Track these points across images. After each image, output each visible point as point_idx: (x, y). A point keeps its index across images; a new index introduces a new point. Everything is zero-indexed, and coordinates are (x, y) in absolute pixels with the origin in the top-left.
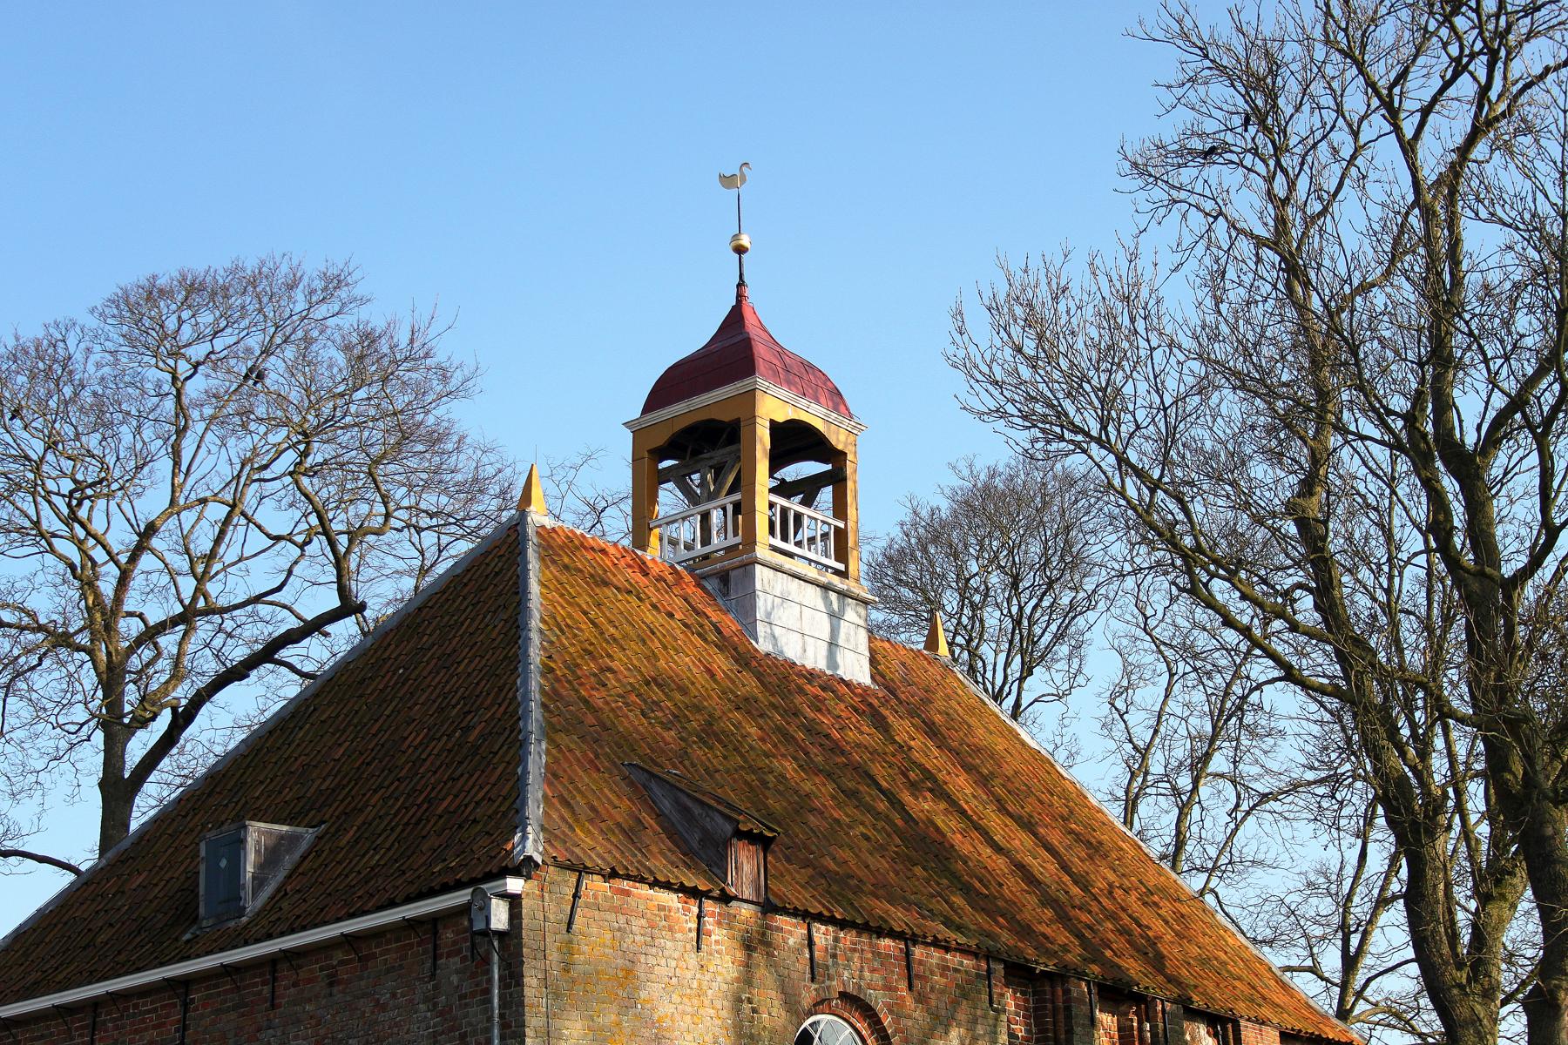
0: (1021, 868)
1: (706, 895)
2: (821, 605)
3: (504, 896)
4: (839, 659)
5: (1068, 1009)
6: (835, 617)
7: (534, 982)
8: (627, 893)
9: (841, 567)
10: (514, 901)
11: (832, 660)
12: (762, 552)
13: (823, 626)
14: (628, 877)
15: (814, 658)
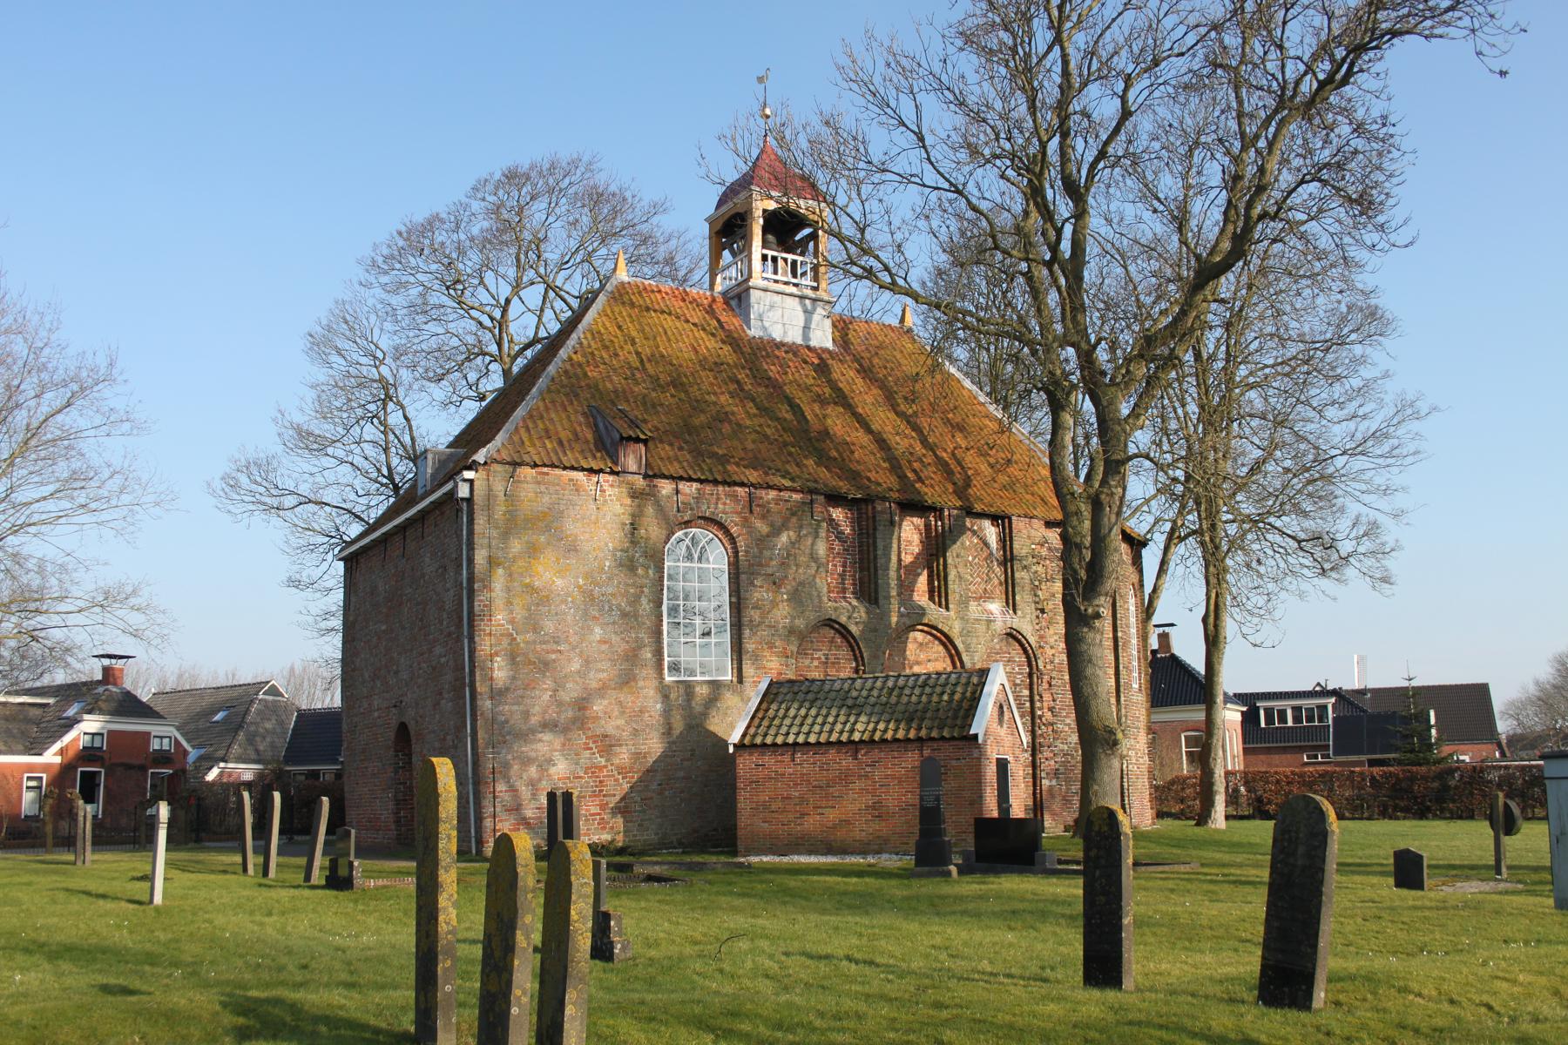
0: (881, 442)
1: (601, 471)
2: (799, 308)
3: (465, 480)
4: (811, 335)
5: (874, 517)
6: (808, 313)
7: (481, 522)
8: (547, 474)
9: (815, 284)
10: (471, 482)
11: (806, 336)
12: (756, 281)
13: (800, 318)
14: (545, 465)
15: (794, 336)
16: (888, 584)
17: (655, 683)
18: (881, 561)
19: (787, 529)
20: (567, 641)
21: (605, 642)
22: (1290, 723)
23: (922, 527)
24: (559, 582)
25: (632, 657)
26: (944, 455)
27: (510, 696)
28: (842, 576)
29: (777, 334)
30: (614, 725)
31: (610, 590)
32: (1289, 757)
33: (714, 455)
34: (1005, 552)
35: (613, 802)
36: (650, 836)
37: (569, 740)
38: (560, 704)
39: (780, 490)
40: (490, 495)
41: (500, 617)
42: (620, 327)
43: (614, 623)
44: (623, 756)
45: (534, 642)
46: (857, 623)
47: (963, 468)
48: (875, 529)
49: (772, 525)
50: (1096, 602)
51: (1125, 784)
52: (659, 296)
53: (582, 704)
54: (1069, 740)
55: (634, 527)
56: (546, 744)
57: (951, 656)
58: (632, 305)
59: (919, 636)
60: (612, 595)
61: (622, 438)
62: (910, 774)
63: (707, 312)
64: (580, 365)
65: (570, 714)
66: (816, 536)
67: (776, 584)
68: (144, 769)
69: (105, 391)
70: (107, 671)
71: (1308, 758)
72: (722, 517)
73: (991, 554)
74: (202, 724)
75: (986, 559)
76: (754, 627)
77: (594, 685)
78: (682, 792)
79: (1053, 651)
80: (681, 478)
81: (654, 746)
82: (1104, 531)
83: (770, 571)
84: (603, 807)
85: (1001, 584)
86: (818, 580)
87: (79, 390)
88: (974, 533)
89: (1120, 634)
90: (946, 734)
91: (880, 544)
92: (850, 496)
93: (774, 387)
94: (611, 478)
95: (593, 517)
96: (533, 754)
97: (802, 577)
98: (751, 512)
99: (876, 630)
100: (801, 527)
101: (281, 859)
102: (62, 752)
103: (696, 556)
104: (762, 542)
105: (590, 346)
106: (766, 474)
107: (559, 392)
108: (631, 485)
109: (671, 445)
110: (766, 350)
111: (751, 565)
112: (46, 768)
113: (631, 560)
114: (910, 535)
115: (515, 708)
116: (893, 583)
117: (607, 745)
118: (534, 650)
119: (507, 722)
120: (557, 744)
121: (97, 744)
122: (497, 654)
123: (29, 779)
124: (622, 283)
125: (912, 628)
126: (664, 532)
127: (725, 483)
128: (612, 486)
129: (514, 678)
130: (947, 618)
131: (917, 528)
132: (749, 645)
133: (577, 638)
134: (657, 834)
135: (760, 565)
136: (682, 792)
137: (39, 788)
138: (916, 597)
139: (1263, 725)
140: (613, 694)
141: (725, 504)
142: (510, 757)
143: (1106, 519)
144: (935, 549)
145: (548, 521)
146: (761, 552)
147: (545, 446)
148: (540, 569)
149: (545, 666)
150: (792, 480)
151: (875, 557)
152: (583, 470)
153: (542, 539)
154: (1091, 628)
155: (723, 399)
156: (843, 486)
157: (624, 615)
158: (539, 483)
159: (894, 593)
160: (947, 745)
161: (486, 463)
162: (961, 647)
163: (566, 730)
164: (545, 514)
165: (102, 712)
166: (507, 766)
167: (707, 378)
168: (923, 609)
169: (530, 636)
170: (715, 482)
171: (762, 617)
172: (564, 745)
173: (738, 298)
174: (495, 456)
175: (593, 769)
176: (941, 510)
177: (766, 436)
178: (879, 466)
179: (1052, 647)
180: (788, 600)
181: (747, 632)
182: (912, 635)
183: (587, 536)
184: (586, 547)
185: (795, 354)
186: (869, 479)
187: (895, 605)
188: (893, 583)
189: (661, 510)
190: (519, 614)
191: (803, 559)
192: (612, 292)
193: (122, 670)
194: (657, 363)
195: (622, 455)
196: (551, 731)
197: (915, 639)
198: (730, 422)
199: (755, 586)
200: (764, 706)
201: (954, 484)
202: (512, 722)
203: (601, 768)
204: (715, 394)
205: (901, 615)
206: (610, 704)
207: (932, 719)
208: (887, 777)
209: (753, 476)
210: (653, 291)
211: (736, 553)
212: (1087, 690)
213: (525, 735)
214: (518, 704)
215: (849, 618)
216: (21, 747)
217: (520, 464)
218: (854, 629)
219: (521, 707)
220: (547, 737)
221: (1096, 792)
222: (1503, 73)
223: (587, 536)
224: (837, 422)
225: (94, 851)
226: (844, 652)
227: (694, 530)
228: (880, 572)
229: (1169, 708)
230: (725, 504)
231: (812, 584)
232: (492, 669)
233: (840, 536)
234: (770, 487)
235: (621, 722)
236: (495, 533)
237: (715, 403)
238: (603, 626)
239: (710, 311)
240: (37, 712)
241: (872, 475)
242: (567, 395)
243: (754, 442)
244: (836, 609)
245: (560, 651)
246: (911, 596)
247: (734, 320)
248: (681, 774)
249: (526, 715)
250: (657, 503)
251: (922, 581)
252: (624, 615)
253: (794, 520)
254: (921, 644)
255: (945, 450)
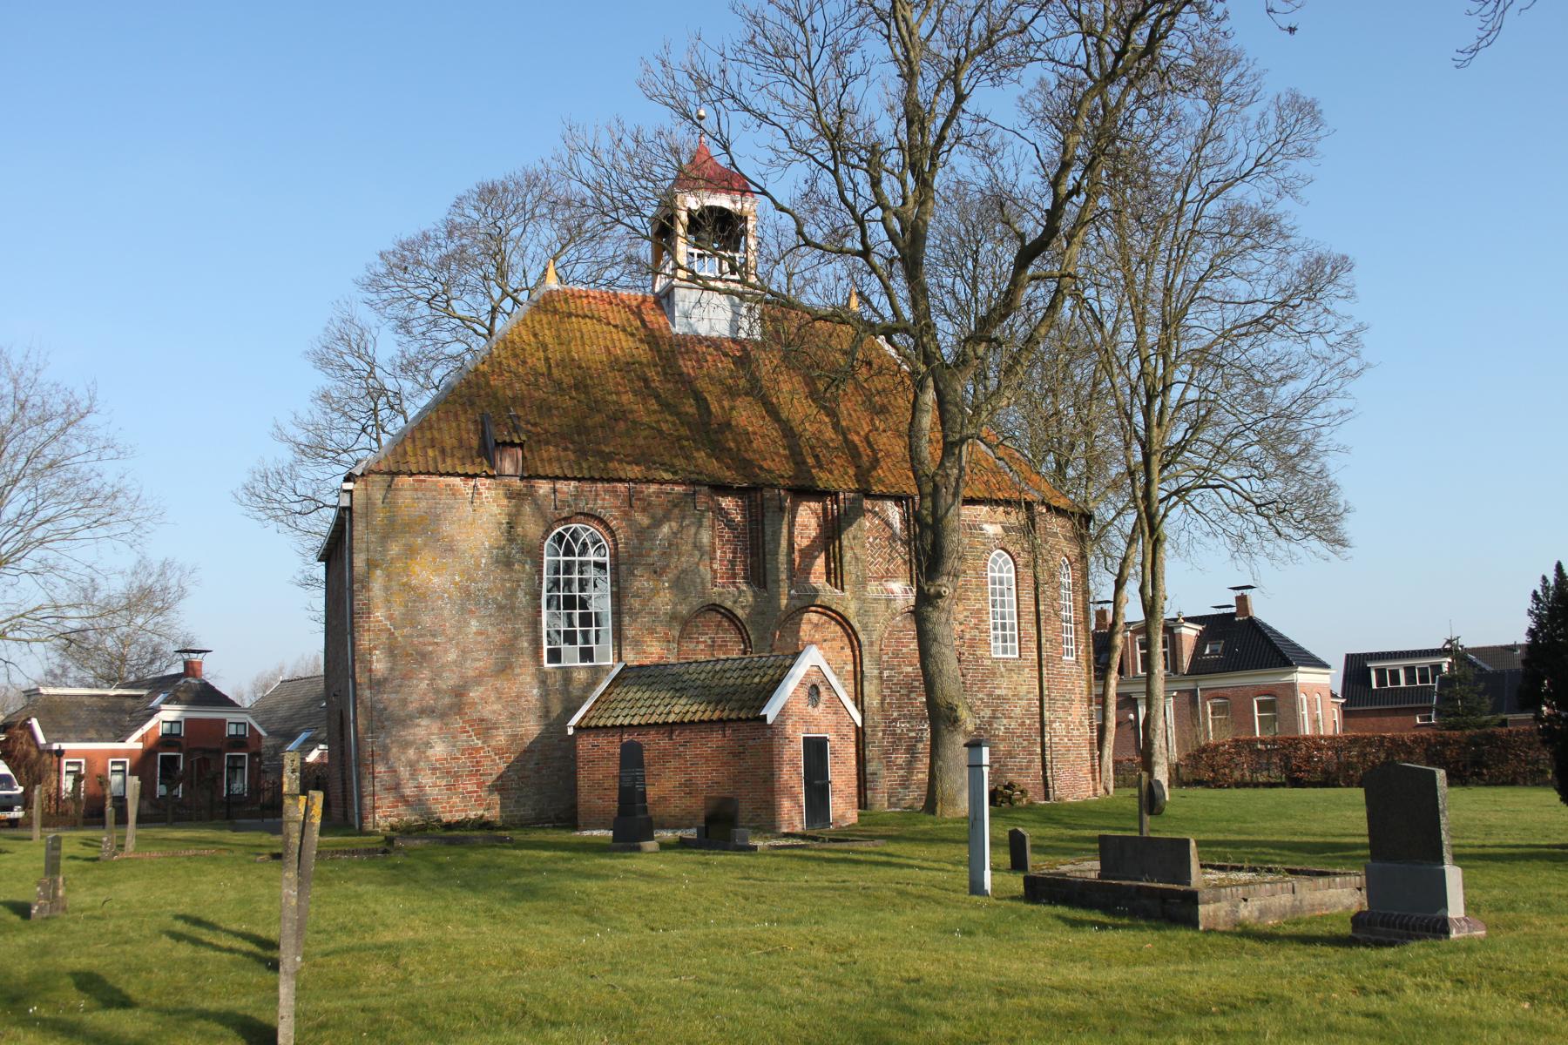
1: (475, 476)
8: (424, 481)
14: (420, 473)
16: (778, 568)
17: (531, 669)
18: (769, 547)
19: (669, 520)
20: (443, 633)
21: (481, 634)
22: (1403, 684)
23: (820, 511)
24: (435, 580)
25: (509, 647)
26: (856, 438)
27: (388, 687)
28: (732, 562)
29: (703, 329)
30: (491, 709)
31: (486, 585)
32: (1399, 720)
33: (600, 453)
34: (909, 531)
35: (490, 780)
36: (527, 811)
37: (446, 724)
38: (437, 691)
39: (662, 484)
40: (369, 504)
41: (379, 614)
42: (535, 335)
43: (490, 616)
44: (501, 738)
45: (411, 636)
46: (743, 607)
47: (873, 450)
48: (763, 516)
49: (653, 517)
50: (939, 582)
51: (1048, 758)
52: (585, 301)
53: (459, 692)
54: (982, 714)
55: (511, 526)
56: (424, 728)
57: (849, 636)
58: (555, 312)
59: (814, 617)
60: (488, 589)
61: (497, 444)
62: (716, 754)
63: (633, 313)
64: (484, 374)
65: (447, 700)
66: (700, 526)
67: (657, 573)
68: (220, 753)
69: (90, 420)
70: (187, 664)
71: (1422, 719)
72: (600, 512)
73: (894, 534)
74: (313, 710)
75: (888, 539)
76: (634, 615)
77: (471, 673)
78: (560, 770)
79: (962, 627)
80: (557, 478)
81: (532, 728)
82: (941, 512)
83: (650, 560)
84: (480, 785)
85: (905, 563)
86: (701, 567)
87: (73, 417)
88: (876, 514)
89: (1042, 608)
90: (743, 715)
91: (769, 531)
92: (735, 486)
93: (683, 383)
94: (488, 481)
95: (470, 519)
96: (411, 738)
97: (685, 565)
98: (631, 506)
99: (763, 613)
100: (684, 518)
101: (140, 832)
102: (143, 739)
103: (577, 551)
104: (643, 534)
105: (499, 356)
106: (649, 469)
107: (455, 402)
108: (507, 487)
109: (556, 446)
110: (686, 346)
111: (630, 556)
112: (129, 753)
113: (508, 556)
114: (807, 518)
115: (393, 696)
116: (783, 567)
117: (485, 728)
118: (412, 644)
119: (385, 709)
120: (435, 727)
121: (176, 731)
122: (375, 648)
123: (113, 763)
124: (551, 292)
125: (805, 609)
126: (542, 529)
127: (602, 480)
128: (488, 489)
129: (392, 669)
130: (843, 599)
131: (814, 512)
132: (630, 632)
133: (454, 631)
134: (534, 810)
135: (641, 555)
136: (560, 770)
137: (124, 771)
138: (812, 579)
139: (1374, 686)
140: (490, 682)
141: (605, 500)
142: (388, 741)
143: (942, 501)
144: (832, 532)
145: (427, 526)
146: (641, 544)
147: (426, 455)
148: (417, 569)
149: (423, 657)
150: (675, 473)
151: (764, 544)
152: (459, 475)
153: (419, 541)
154: (936, 607)
155: (624, 398)
156: (728, 475)
157: (500, 608)
158: (416, 490)
159: (783, 576)
160: (744, 726)
161: (363, 475)
162: (857, 626)
163: (443, 716)
164: (422, 518)
165: (179, 702)
166: (386, 749)
167: (613, 377)
168: (816, 590)
169: (407, 631)
170: (593, 480)
171: (644, 605)
172: (441, 729)
173: (665, 300)
174: (373, 467)
175: (472, 751)
176: (836, 494)
177: (660, 432)
178: (778, 454)
179: (961, 624)
180: (669, 588)
181: (626, 620)
182: (806, 616)
183: (464, 536)
184: (462, 546)
185: (717, 348)
186: (761, 468)
187: (784, 588)
188: (783, 567)
189: (538, 508)
190: (398, 611)
191: (686, 548)
192: (538, 301)
193: (200, 663)
194: (564, 367)
195: (498, 458)
196: (428, 716)
197: (810, 621)
198: (626, 420)
199: (634, 575)
200: (610, 690)
201: (858, 467)
202: (390, 709)
203: (478, 750)
204: (618, 393)
205: (791, 598)
206: (487, 690)
207: (737, 701)
208: (696, 756)
209: (635, 471)
210: (581, 297)
211: (616, 545)
212: (932, 668)
213: (404, 722)
214: (397, 692)
215: (735, 602)
216: (111, 735)
217: (399, 473)
218: (740, 613)
219: (400, 696)
220: (424, 722)
221: (941, 767)
222: (1292, 30)
223: (464, 536)
224: (746, 415)
225: (137, 828)
226: (732, 636)
227: (574, 526)
228: (768, 557)
229: (1219, 675)
230: (604, 499)
231: (697, 572)
232: (371, 662)
233: (730, 523)
234: (653, 481)
235: (497, 707)
236: (373, 538)
237: (616, 403)
238: (479, 619)
239: (638, 313)
240: (129, 703)
241: (767, 464)
242: (463, 405)
243: (645, 438)
244: (720, 594)
245: (437, 644)
246: (807, 578)
247: (660, 319)
248: (559, 754)
249: (404, 702)
250: (535, 501)
251: (819, 564)
252: (500, 608)
253: (676, 511)
254: (817, 625)
255: (858, 434)
